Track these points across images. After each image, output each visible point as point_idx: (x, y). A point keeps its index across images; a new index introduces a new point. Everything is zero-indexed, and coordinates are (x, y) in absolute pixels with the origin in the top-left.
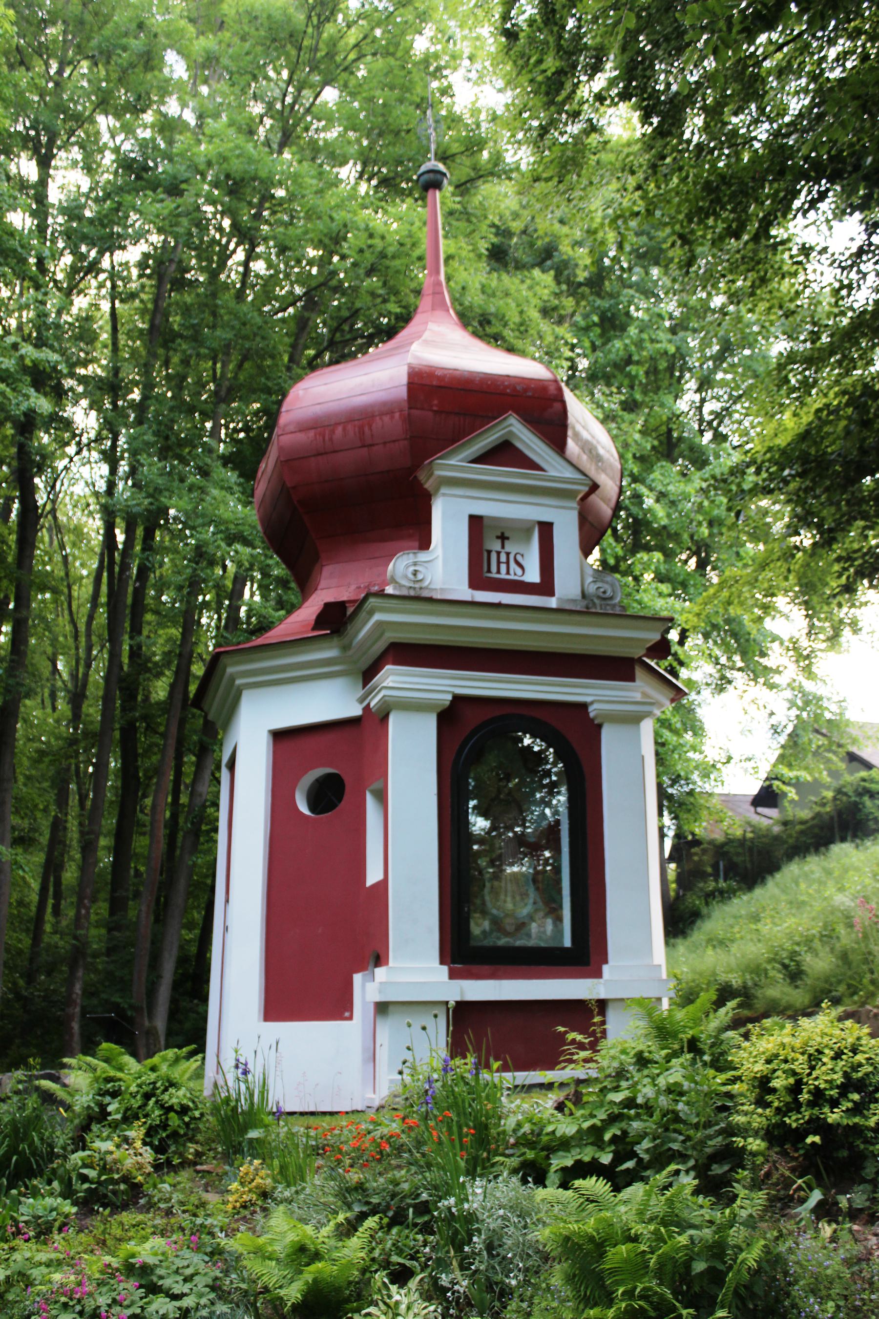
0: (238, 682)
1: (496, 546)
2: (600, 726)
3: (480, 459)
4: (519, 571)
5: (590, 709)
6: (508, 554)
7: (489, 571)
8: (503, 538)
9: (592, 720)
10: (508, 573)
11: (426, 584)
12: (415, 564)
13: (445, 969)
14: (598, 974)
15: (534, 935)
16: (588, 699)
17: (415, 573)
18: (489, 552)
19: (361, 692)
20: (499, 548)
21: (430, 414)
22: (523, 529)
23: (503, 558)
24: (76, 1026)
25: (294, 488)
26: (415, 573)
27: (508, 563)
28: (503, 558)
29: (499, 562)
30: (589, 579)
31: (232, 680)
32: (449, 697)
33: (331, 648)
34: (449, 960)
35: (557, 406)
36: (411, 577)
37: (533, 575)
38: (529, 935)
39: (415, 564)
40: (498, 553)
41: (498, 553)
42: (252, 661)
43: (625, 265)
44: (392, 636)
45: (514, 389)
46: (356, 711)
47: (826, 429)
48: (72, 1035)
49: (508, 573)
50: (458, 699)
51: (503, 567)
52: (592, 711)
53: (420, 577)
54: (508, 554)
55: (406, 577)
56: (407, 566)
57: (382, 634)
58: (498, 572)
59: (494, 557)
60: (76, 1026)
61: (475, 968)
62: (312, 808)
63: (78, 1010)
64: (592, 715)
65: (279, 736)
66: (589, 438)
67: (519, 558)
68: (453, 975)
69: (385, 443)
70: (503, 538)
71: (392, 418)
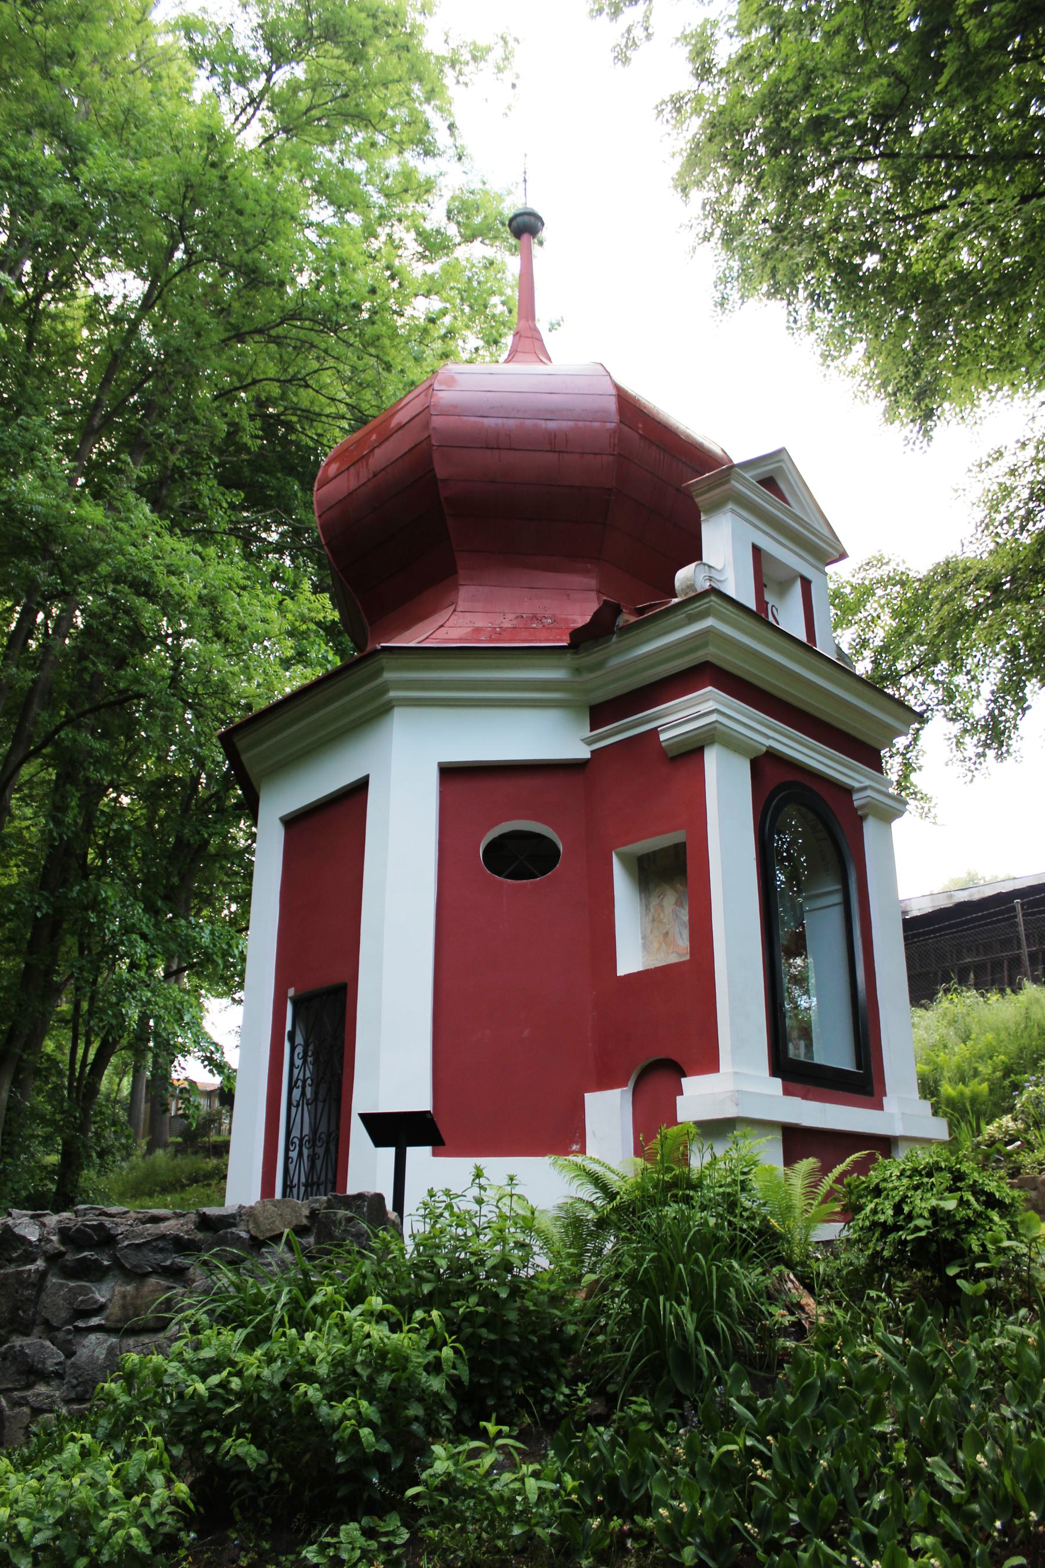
0: (392, 694)
2: (861, 819)
5: (855, 797)
9: (855, 810)
13: (778, 1082)
16: (856, 785)
19: (588, 734)
25: (444, 481)
31: (384, 689)
32: (764, 749)
33: (558, 667)
43: (187, 643)
44: (711, 653)
46: (583, 753)
47: (934, 591)
52: (858, 800)
57: (705, 645)
64: (856, 804)
65: (449, 773)
68: (787, 1092)
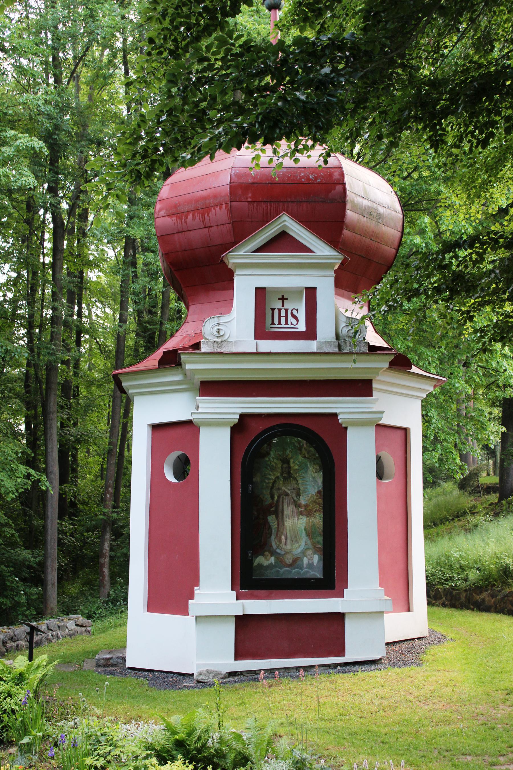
1: (278, 305)
2: (346, 428)
3: (260, 249)
4: (294, 322)
5: (339, 417)
6: (286, 310)
7: (273, 323)
8: (283, 299)
9: (341, 425)
10: (286, 323)
11: (225, 338)
12: (218, 324)
14: (341, 595)
15: (305, 566)
16: (337, 411)
17: (218, 331)
18: (273, 310)
20: (280, 307)
21: (247, 203)
22: (295, 292)
23: (283, 313)
24: (106, 570)
26: (218, 331)
27: (286, 316)
28: (283, 313)
29: (280, 317)
30: (342, 325)
32: (238, 417)
34: (238, 587)
35: (339, 188)
36: (216, 334)
37: (302, 327)
38: (301, 568)
39: (218, 324)
40: (280, 310)
41: (280, 310)
42: (135, 379)
45: (308, 179)
48: (104, 576)
49: (286, 323)
50: (243, 416)
51: (283, 320)
52: (341, 418)
53: (222, 333)
54: (286, 310)
55: (212, 334)
56: (213, 327)
58: (280, 323)
59: (276, 312)
60: (106, 570)
61: (256, 592)
62: (176, 476)
63: (107, 560)
64: (340, 421)
65: (156, 428)
66: (369, 204)
67: (294, 312)
69: (217, 225)
70: (283, 299)
71: (221, 208)
